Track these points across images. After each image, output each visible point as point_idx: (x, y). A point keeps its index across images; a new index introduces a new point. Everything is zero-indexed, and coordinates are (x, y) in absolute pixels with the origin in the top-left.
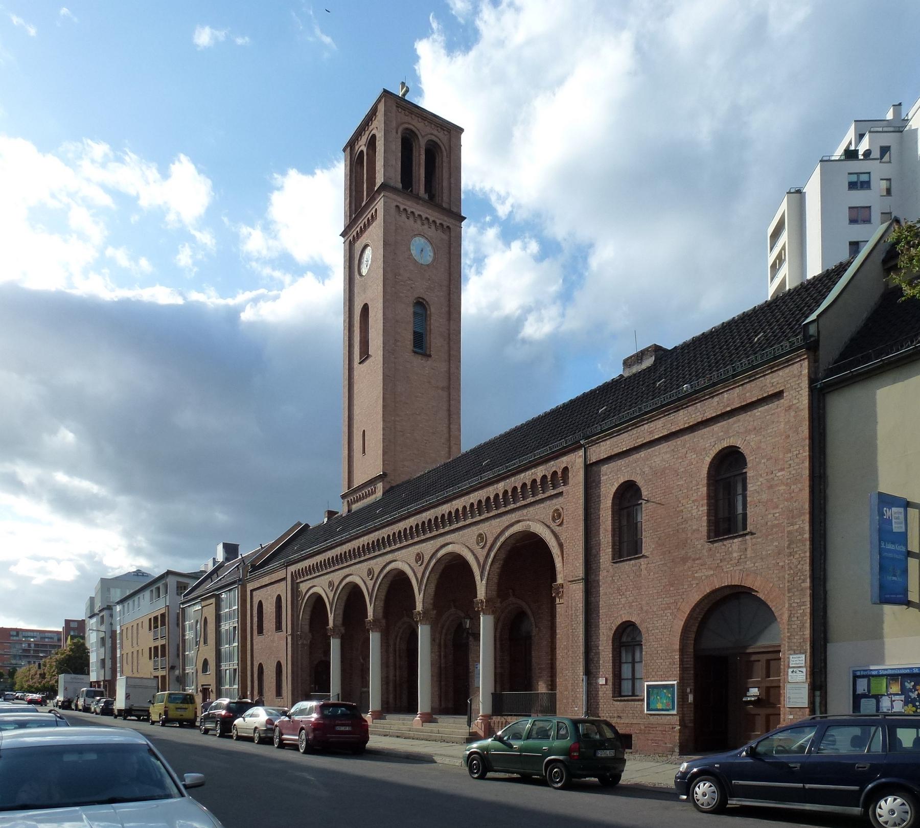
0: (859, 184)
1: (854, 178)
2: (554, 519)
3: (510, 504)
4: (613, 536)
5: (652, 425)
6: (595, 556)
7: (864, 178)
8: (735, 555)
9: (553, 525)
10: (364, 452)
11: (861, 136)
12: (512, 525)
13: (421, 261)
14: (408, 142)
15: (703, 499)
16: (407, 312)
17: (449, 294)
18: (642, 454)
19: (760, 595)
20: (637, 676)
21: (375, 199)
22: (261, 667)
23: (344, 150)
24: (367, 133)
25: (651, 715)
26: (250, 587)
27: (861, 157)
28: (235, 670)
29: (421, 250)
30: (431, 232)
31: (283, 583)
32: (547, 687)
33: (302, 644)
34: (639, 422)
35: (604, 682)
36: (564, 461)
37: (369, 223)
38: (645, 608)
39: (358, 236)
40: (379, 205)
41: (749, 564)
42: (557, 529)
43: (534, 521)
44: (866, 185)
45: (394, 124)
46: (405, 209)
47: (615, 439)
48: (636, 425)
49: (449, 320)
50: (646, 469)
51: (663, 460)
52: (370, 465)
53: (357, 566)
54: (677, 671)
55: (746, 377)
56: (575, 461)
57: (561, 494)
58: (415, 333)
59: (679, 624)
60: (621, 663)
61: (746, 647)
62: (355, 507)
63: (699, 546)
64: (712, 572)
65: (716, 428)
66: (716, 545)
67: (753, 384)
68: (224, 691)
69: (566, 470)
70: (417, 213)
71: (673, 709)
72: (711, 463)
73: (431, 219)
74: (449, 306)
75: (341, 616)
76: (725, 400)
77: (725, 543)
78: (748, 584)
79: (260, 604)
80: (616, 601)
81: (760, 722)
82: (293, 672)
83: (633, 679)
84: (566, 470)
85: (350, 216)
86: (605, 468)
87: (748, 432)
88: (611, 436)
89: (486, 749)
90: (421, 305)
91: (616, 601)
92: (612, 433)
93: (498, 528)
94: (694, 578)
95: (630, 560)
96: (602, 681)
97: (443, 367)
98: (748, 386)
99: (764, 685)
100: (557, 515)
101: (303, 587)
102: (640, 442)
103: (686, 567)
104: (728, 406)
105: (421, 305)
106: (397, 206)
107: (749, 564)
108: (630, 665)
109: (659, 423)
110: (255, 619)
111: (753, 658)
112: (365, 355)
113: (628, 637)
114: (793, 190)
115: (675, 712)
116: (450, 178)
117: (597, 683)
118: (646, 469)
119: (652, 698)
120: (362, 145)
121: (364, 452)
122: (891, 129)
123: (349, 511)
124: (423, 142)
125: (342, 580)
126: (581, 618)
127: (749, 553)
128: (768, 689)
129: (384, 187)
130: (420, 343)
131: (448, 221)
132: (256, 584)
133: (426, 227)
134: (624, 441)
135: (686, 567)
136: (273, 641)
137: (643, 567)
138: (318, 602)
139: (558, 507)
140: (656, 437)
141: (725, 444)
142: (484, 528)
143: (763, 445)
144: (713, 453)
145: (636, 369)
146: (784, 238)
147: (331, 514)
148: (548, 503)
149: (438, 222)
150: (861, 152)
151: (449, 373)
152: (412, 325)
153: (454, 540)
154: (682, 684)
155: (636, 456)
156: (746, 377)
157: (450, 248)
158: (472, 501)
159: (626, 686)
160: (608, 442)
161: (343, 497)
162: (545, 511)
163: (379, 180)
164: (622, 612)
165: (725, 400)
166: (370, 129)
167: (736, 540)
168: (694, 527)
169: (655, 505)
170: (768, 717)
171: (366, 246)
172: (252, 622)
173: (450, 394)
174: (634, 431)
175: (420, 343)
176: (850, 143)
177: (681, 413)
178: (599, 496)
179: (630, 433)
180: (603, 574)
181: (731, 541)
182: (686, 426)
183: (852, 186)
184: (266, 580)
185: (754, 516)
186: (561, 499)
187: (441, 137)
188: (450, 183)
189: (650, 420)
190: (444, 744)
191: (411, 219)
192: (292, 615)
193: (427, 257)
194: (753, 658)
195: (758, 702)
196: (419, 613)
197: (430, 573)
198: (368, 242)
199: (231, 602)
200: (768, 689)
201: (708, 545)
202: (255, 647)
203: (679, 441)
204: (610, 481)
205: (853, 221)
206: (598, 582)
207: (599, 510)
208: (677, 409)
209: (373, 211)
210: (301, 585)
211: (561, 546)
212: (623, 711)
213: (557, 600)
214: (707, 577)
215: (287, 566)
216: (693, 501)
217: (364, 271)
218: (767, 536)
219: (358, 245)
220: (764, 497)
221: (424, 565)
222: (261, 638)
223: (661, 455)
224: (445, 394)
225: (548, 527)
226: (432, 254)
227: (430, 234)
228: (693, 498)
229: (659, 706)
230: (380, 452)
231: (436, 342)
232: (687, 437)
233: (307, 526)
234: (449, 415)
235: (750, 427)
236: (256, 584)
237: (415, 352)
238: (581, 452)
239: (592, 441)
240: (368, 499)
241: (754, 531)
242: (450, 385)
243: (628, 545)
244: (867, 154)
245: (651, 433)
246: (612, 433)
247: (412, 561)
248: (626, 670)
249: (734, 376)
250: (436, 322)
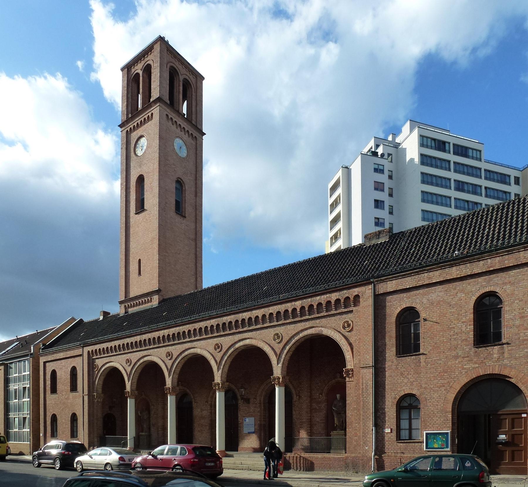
0: (379, 170)
1: (376, 167)
2: (344, 327)
3: (305, 315)
4: (396, 340)
5: (431, 274)
6: (382, 352)
7: (381, 167)
8: (495, 356)
9: (343, 331)
10: (140, 273)
11: (377, 146)
12: (306, 329)
13: (180, 155)
14: (173, 74)
15: (470, 321)
16: (173, 186)
17: (196, 180)
18: (421, 291)
19: (512, 380)
20: (413, 427)
21: (151, 107)
22: (54, 418)
23: (122, 70)
24: (143, 62)
25: (429, 451)
26: (42, 360)
27: (379, 156)
28: (25, 419)
29: (180, 146)
30: (186, 137)
31: (79, 359)
32: (307, 433)
33: (98, 401)
34: (421, 271)
35: (389, 431)
36: (355, 291)
37: (145, 122)
38: (423, 386)
39: (135, 128)
40: (156, 110)
41: (506, 361)
42: (347, 334)
43: (329, 328)
44: (382, 171)
45: (165, 61)
46: (171, 118)
47: (400, 280)
48: (418, 273)
49: (196, 196)
50: (425, 301)
51: (438, 296)
52: (146, 282)
53: (156, 350)
54: (450, 424)
55: (506, 251)
56: (366, 293)
57: (351, 312)
58: (176, 200)
59: (451, 396)
60: (400, 419)
61: (498, 411)
62: (131, 310)
63: (467, 350)
64: (477, 365)
65: (480, 279)
66: (480, 349)
67: (510, 256)
68: (12, 435)
69: (357, 297)
70: (178, 123)
71: (447, 447)
72: (476, 300)
73: (186, 129)
74: (196, 187)
75: (135, 383)
76: (489, 263)
77: (488, 348)
78: (505, 372)
79: (54, 373)
80: (399, 381)
81: (507, 454)
82: (89, 421)
83: (410, 429)
84: (357, 297)
85: (127, 115)
86: (389, 298)
87: (505, 284)
88: (396, 278)
89: (145, 460)
90: (179, 182)
91: (399, 381)
92: (398, 276)
93: (293, 332)
94: (463, 369)
95: (412, 356)
96: (388, 430)
97: (193, 226)
98: (507, 257)
99: (511, 433)
100: (347, 325)
101: (99, 362)
102: (420, 283)
103: (457, 362)
104: (491, 267)
105: (179, 182)
106: (167, 115)
107: (506, 361)
108: (408, 421)
109: (437, 273)
110: (48, 383)
111: (502, 417)
112: (141, 207)
113: (408, 404)
114: (344, 166)
115: (449, 449)
116: (196, 106)
117: (383, 432)
118: (425, 301)
119: (429, 441)
120: (138, 69)
121: (140, 273)
122: (392, 145)
123: (125, 313)
124: (181, 78)
125: (138, 360)
126: (371, 391)
127: (506, 355)
128: (513, 435)
129: (159, 100)
130: (179, 208)
131: (196, 134)
132: (50, 358)
133: (183, 133)
134: (408, 282)
135: (457, 362)
136: (67, 399)
137: (422, 360)
138: (114, 374)
139: (348, 320)
140: (434, 281)
141: (487, 290)
142: (280, 330)
143: (516, 292)
144: (478, 295)
145: (374, 242)
146: (339, 191)
147: (106, 314)
148: (339, 317)
149: (190, 132)
150: (379, 154)
151: (196, 230)
152: (174, 195)
153: (251, 336)
154: (452, 432)
155: (412, 293)
156: (506, 251)
157: (196, 150)
158: (271, 311)
159: (405, 434)
160: (394, 282)
161: (121, 303)
162: (338, 321)
163: (155, 94)
164: (404, 388)
165: (489, 263)
166: (146, 59)
167: (496, 347)
168: (463, 338)
169: (432, 323)
170: (513, 452)
171: (141, 137)
172: (43, 386)
173: (196, 244)
174: (416, 277)
175: (179, 208)
176: (372, 148)
177: (454, 268)
178: (385, 315)
179: (413, 277)
180: (388, 364)
181: (492, 347)
182: (459, 276)
183: (376, 170)
184: (61, 355)
185: (506, 333)
186: (350, 315)
187: (192, 79)
188: (196, 110)
189: (429, 271)
190: (251, 472)
191: (175, 125)
192: (89, 381)
193: (183, 153)
194: (502, 417)
195: (506, 444)
196: (218, 384)
197: (228, 357)
198: (144, 134)
199: (22, 370)
200: (513, 435)
201: (473, 350)
202: (47, 402)
203: (451, 285)
204: (395, 306)
205: (376, 189)
206: (384, 368)
207: (385, 324)
208: (451, 266)
209: (150, 114)
210: (97, 360)
211: (350, 344)
212: (406, 449)
213: (347, 379)
214: (474, 368)
215: (83, 347)
216: (463, 322)
217: (139, 152)
218: (519, 346)
219: (134, 136)
220: (517, 322)
221: (222, 352)
222: (54, 396)
223: (437, 293)
224: (193, 243)
225: (339, 332)
226: (186, 152)
227: (185, 139)
228: (463, 321)
229: (436, 446)
230: (156, 275)
231: (189, 209)
232: (457, 283)
233: (81, 320)
234: (196, 257)
235: (506, 281)
236: (50, 358)
237: (176, 213)
238: (371, 287)
239: (381, 280)
240: (141, 306)
241: (510, 342)
242: (196, 238)
243: (408, 345)
244: (383, 155)
245: (430, 278)
246: (398, 276)
247: (211, 349)
248: (405, 424)
249: (496, 250)
250: (189, 196)
